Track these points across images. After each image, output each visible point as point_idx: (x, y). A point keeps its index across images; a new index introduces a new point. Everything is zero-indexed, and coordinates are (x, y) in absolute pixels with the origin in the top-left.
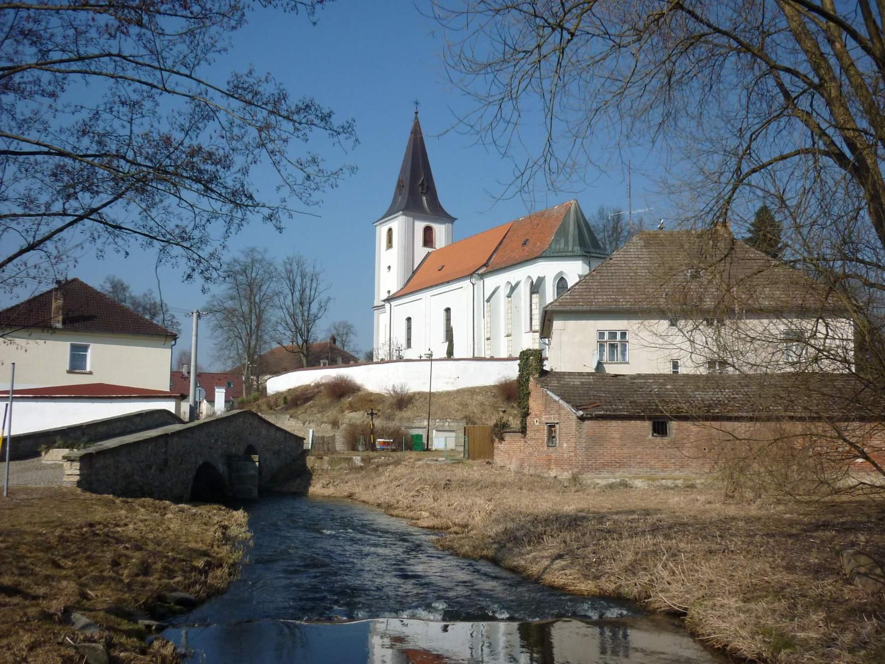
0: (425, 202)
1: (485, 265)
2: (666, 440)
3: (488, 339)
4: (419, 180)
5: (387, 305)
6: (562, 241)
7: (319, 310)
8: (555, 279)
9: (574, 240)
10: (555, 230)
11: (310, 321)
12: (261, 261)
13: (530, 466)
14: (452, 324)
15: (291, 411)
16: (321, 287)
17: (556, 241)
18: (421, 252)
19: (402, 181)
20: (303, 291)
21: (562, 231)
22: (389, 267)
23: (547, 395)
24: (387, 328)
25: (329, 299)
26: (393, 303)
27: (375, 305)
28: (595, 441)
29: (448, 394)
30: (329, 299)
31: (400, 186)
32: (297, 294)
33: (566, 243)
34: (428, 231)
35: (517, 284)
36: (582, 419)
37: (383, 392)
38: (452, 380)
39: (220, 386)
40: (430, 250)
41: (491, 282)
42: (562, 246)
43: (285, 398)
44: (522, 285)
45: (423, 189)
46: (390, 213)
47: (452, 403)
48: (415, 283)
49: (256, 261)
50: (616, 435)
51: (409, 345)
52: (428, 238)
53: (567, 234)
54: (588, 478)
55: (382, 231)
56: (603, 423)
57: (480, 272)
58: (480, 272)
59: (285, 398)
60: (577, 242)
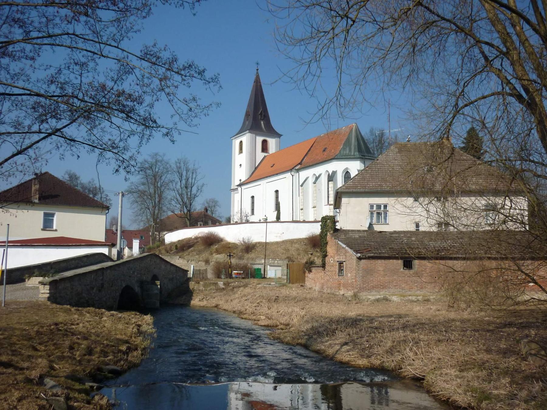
0: (263, 125)
1: (299, 164)
2: (412, 272)
3: (302, 209)
4: (259, 111)
5: (239, 189)
6: (348, 149)
7: (197, 191)
8: (343, 172)
9: (355, 148)
10: (343, 142)
11: (192, 198)
12: (161, 161)
13: (327, 288)
14: (280, 200)
15: (180, 254)
16: (199, 177)
17: (344, 149)
18: (260, 155)
19: (249, 112)
20: (187, 180)
21: (348, 143)
22: (241, 165)
23: (338, 244)
24: (239, 203)
25: (203, 185)
26: (243, 187)
27: (232, 188)
28: (368, 272)
29: (277, 243)
30: (203, 185)
31: (247, 115)
32: (184, 182)
33: (350, 150)
34: (265, 143)
35: (320, 175)
36: (360, 259)
37: (237, 242)
38: (279, 235)
39: (136, 238)
40: (266, 154)
41: (304, 174)
42: (347, 152)
43: (176, 246)
44: (322, 176)
45: (261, 117)
46: (241, 132)
47: (279, 249)
48: (257, 175)
49: (158, 161)
50: (381, 269)
51: (253, 213)
52: (265, 147)
53: (351, 145)
54: (363, 295)
55: (236, 142)
56: (372, 261)
57: (297, 168)
58: (297, 168)
59: (176, 246)
60: (357, 149)
